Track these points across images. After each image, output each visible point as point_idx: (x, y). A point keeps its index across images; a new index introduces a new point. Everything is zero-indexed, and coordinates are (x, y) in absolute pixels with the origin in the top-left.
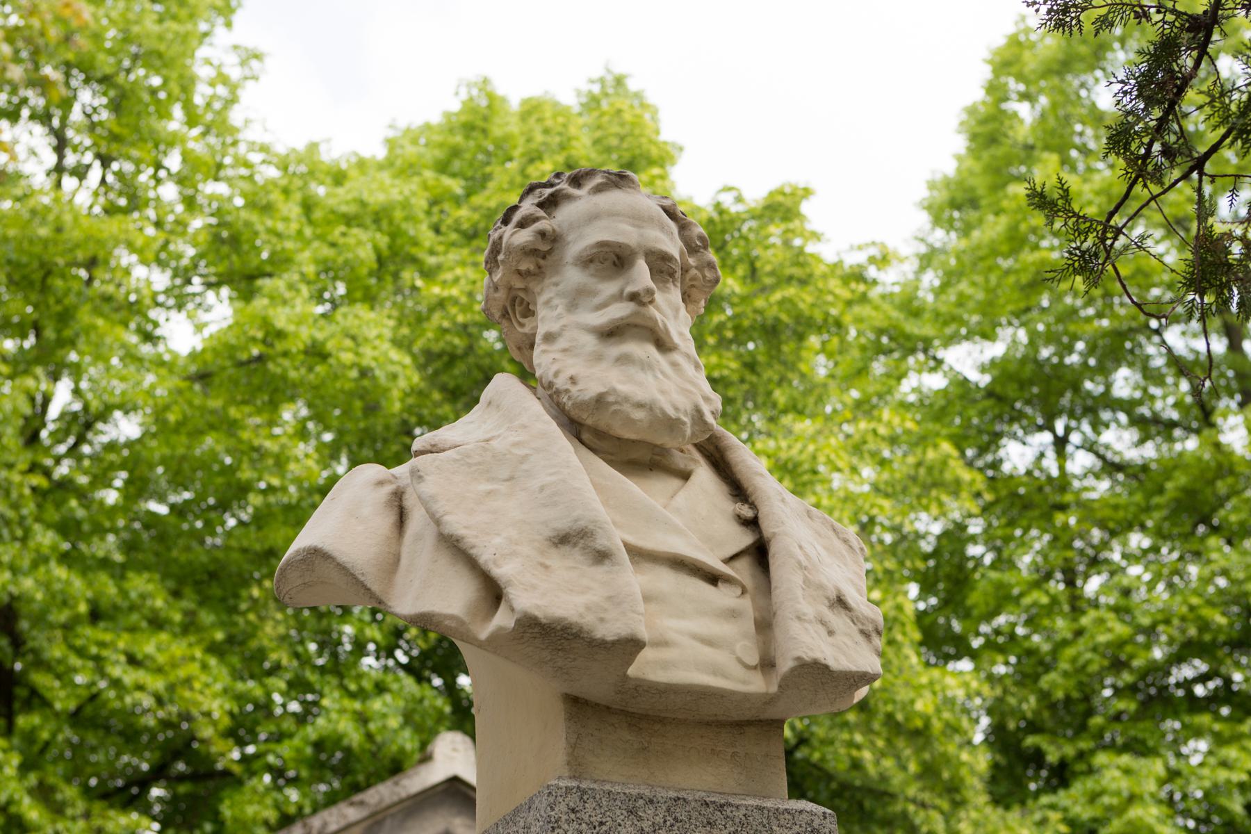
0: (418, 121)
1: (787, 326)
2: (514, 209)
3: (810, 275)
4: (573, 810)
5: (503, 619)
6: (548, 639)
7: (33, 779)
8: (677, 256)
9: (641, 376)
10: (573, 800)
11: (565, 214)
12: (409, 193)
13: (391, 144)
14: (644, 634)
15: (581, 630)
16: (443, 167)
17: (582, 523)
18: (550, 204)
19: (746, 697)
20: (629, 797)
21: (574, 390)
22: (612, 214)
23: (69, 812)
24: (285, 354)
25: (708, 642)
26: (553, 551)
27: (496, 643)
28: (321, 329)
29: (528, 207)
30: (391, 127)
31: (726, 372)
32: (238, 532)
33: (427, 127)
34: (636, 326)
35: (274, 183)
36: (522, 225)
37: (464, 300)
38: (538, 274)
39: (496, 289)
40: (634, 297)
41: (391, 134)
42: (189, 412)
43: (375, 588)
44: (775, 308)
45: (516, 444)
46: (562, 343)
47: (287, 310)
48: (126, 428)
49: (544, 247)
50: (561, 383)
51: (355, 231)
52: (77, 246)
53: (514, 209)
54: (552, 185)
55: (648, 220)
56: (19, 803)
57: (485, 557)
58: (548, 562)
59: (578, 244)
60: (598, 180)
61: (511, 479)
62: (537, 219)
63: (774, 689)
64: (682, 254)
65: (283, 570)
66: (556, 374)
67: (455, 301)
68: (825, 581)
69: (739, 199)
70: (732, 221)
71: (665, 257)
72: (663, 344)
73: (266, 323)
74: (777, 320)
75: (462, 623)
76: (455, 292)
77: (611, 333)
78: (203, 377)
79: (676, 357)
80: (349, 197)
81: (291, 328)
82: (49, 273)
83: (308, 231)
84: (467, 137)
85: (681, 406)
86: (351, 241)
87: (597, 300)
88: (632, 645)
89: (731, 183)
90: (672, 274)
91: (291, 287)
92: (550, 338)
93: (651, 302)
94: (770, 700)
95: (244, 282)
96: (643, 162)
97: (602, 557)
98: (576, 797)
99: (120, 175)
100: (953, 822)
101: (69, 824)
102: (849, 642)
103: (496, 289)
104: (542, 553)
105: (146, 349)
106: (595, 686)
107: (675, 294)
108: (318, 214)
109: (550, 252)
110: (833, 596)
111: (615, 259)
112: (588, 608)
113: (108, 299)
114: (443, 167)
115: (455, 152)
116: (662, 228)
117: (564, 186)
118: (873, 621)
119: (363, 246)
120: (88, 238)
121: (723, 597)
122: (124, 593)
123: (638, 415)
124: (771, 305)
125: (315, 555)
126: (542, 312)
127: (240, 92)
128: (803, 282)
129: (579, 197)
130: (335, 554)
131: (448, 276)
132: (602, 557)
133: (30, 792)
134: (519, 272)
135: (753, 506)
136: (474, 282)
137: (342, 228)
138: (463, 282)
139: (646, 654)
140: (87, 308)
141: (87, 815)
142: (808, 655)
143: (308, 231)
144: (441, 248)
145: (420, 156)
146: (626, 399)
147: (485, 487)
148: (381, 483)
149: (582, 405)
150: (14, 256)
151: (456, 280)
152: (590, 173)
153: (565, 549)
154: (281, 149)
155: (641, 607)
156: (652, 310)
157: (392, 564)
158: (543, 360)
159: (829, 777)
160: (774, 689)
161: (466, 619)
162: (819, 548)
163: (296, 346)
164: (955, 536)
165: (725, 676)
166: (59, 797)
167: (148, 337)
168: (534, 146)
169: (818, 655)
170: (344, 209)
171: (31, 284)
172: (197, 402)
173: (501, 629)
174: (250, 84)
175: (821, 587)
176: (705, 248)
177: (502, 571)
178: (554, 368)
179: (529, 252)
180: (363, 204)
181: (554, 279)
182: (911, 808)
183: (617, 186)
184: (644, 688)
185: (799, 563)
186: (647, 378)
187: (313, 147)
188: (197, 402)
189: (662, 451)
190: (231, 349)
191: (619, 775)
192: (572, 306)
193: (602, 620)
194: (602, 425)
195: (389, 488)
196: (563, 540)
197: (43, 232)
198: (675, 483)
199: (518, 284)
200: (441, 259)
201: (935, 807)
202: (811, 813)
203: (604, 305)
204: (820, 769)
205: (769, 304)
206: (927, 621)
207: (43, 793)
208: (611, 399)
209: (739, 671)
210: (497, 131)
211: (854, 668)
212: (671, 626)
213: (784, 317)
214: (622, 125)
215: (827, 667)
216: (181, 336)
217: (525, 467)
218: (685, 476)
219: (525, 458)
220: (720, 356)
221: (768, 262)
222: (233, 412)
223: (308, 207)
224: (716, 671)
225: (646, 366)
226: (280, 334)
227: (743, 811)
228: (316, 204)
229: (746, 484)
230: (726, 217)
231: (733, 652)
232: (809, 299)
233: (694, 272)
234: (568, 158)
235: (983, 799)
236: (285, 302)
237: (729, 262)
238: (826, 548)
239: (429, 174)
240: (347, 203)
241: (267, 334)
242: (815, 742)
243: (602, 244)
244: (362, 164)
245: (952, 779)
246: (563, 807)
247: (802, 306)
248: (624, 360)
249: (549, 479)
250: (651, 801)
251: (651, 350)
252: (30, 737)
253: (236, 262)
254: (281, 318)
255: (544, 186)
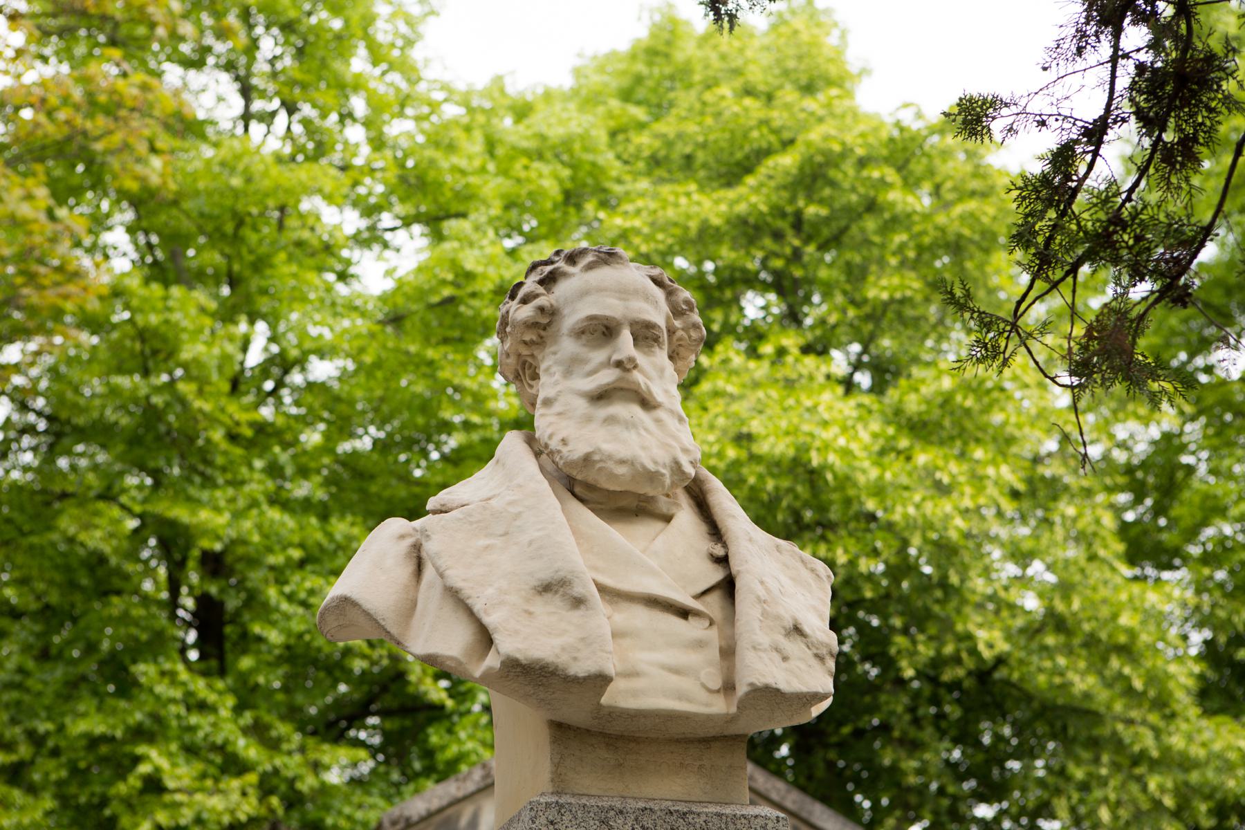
0: (604, 49)
1: (971, 241)
2: (520, 284)
3: (992, 188)
4: (552, 823)
5: (492, 661)
6: (530, 676)
7: (247, 718)
8: (661, 322)
9: (625, 434)
10: (552, 814)
11: (562, 289)
12: (590, 125)
13: (577, 72)
14: (610, 669)
15: (556, 668)
16: (627, 96)
17: (562, 574)
18: (549, 281)
19: (709, 717)
20: (602, 809)
21: (565, 450)
22: (600, 290)
23: (285, 747)
24: (474, 295)
25: (676, 671)
26: (538, 599)
27: (487, 678)
28: (507, 268)
29: (530, 285)
30: (579, 55)
31: (909, 293)
32: (440, 466)
33: (612, 56)
34: (622, 389)
35: (455, 122)
36: (525, 301)
37: (646, 230)
38: (541, 343)
39: (508, 355)
40: (619, 364)
41: (578, 62)
42: (384, 355)
43: (394, 631)
44: (957, 223)
45: (511, 503)
46: (557, 408)
47: (476, 252)
48: (322, 370)
49: (544, 321)
50: (554, 444)
51: (537, 165)
52: (267, 195)
53: (520, 284)
54: (552, 263)
55: (637, 293)
56: (235, 743)
57: (478, 607)
58: (532, 609)
59: (573, 317)
60: (590, 258)
61: (506, 534)
62: (537, 296)
63: (733, 710)
64: (668, 320)
65: (322, 614)
66: (550, 437)
67: (637, 232)
68: (782, 612)
69: (919, 115)
70: (913, 139)
71: (649, 326)
72: (647, 403)
73: (454, 265)
74: (960, 236)
75: (460, 663)
76: (637, 223)
77: (601, 397)
78: (396, 320)
79: (660, 413)
80: (529, 133)
81: (479, 269)
82: (240, 223)
83: (491, 167)
84: (650, 64)
85: (660, 460)
86: (533, 175)
87: (588, 368)
88: (601, 681)
89: (909, 100)
90: (656, 340)
91: (477, 228)
92: (548, 402)
93: (635, 367)
94: (731, 719)
95: (434, 222)
96: (821, 83)
97: (578, 602)
98: (554, 811)
99: (306, 122)
100: (1164, 738)
101: (286, 759)
102: (803, 666)
103: (508, 355)
104: (528, 600)
105: (342, 289)
106: (575, 713)
107: (661, 356)
108: (500, 151)
109: (549, 324)
110: (790, 625)
111: (604, 330)
112: (563, 649)
113: (299, 244)
114: (627, 96)
115: (639, 80)
116: (647, 298)
117: (561, 264)
118: (827, 645)
119: (548, 180)
120: (277, 187)
121: (692, 629)
122: (330, 536)
123: (621, 470)
124: (952, 221)
125: (345, 603)
126: (544, 378)
127: (421, 28)
128: (984, 195)
129: (572, 275)
130: (361, 602)
131: (629, 207)
132: (578, 602)
133: (246, 731)
134: (525, 343)
135: (725, 545)
136: (655, 212)
137: (524, 161)
138: (644, 214)
139: (618, 685)
140: (282, 256)
141: (302, 750)
142: (760, 681)
143: (491, 167)
144: (628, 178)
145: (606, 85)
146: (610, 457)
147: (483, 542)
148: (402, 537)
149: (571, 464)
150: (207, 209)
151: (638, 212)
152: (583, 252)
153: (548, 596)
154: (461, 86)
155: (610, 646)
156: (637, 376)
157: (409, 608)
158: (544, 423)
159: (1028, 698)
160: (733, 710)
161: (463, 660)
162: (784, 579)
163: (486, 287)
164: (1170, 444)
165: (689, 700)
166: (274, 733)
167: (343, 276)
168: (711, 73)
169: (770, 681)
170: (525, 144)
171: (223, 236)
172: (390, 344)
173: (491, 668)
174: (432, 20)
175: (778, 617)
176: (691, 310)
177: (489, 620)
178: (549, 431)
179: (531, 325)
180: (543, 137)
181: (553, 349)
182: (1120, 727)
183: (606, 263)
184: (616, 714)
185: (758, 598)
186: (631, 436)
187: (498, 81)
188: (390, 344)
189: (651, 499)
190: (421, 294)
191: (597, 786)
192: (568, 373)
193: (575, 659)
194: (590, 480)
195: (409, 541)
196: (546, 588)
197: (236, 182)
198: (659, 525)
199: (525, 351)
200: (629, 187)
201: (1144, 722)
202: (766, 817)
203: (594, 372)
204: (1020, 689)
205: (951, 219)
206: (1133, 532)
207: (258, 731)
208: (596, 457)
209: (703, 696)
210: (679, 56)
211: (805, 689)
212: (643, 658)
213: (966, 232)
214: (798, 46)
215: (778, 690)
216: (374, 276)
217: (518, 523)
218: (668, 519)
219: (518, 515)
220: (902, 277)
221: (950, 177)
222: (431, 353)
223: (491, 146)
224: (681, 696)
225: (630, 425)
226: (469, 276)
227: (703, 817)
228: (501, 141)
229: (720, 525)
230: (906, 135)
231: (698, 678)
232: (991, 211)
233: (680, 333)
234: (747, 82)
235: (1194, 712)
236: (471, 244)
237: (911, 180)
238: (792, 579)
239: (615, 103)
240: (527, 138)
241: (457, 276)
242: (1013, 662)
243: (591, 318)
244: (548, 96)
245: (1160, 695)
246: (543, 820)
247: (985, 220)
248: (611, 420)
249: (537, 534)
250: (621, 812)
251: (636, 410)
252: (243, 677)
253: (430, 201)
254: (470, 261)
255: (546, 263)
